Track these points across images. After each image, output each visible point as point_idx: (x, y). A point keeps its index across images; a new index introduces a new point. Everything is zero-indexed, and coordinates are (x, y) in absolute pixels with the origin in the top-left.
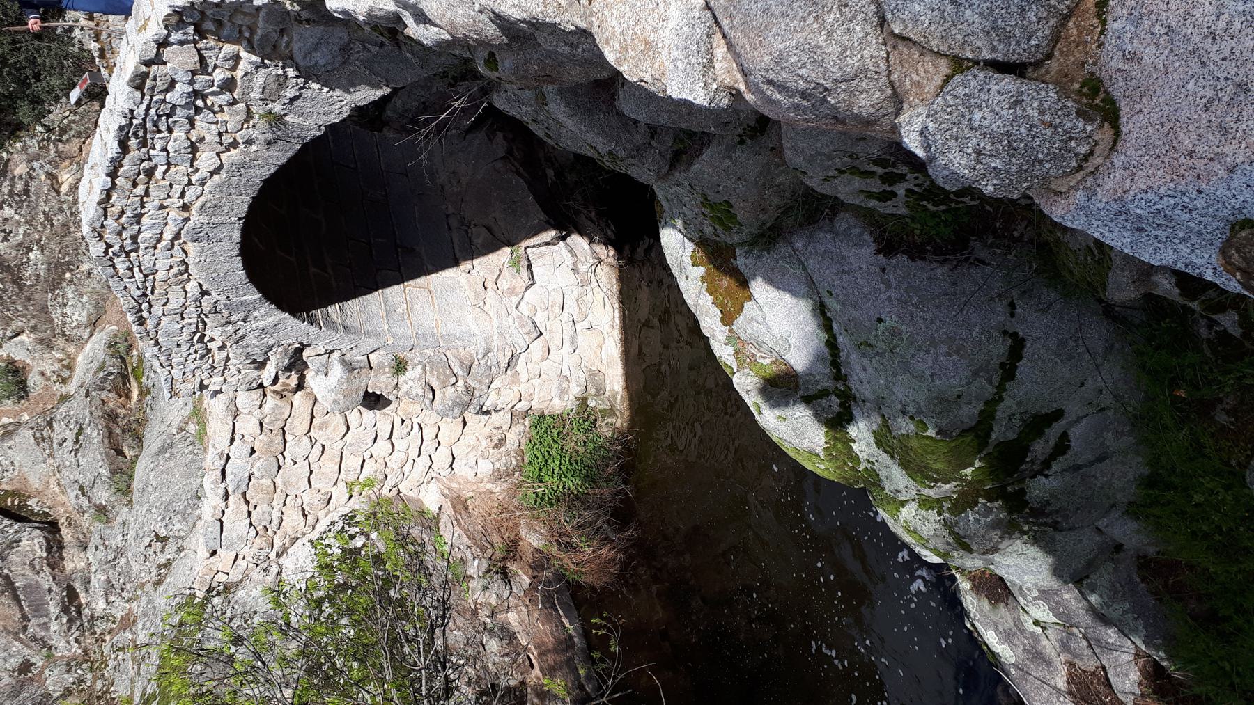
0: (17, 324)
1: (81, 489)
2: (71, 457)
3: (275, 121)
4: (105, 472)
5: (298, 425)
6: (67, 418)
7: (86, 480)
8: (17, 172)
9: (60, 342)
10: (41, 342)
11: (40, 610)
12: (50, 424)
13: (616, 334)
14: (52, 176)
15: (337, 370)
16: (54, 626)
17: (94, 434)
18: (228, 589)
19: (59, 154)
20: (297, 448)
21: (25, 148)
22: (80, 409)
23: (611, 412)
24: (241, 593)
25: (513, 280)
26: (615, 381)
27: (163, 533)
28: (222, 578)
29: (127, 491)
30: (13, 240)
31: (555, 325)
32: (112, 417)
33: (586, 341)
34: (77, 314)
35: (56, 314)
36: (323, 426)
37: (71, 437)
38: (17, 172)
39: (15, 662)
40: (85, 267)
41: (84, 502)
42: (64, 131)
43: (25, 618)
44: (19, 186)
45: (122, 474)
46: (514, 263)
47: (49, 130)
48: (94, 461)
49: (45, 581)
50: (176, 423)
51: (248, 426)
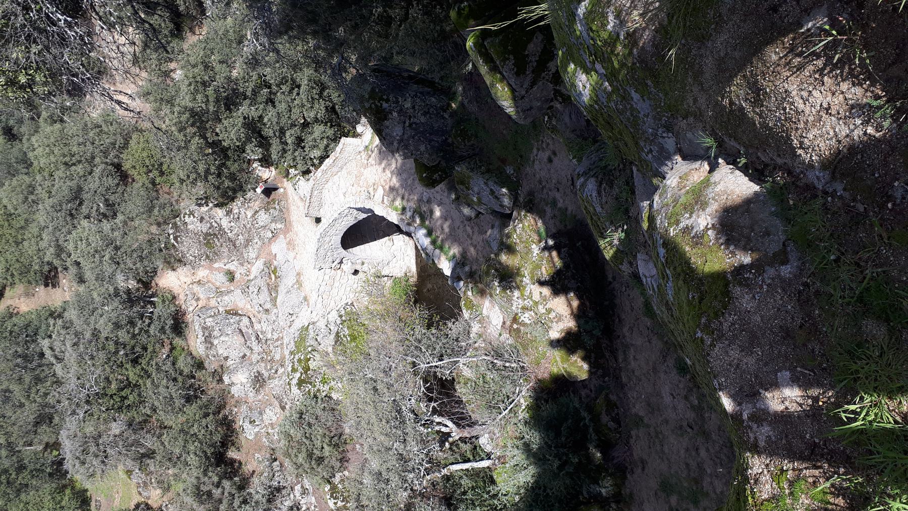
0: (233, 258)
1: (260, 305)
2: (256, 297)
3: (356, 218)
4: (268, 299)
5: (338, 278)
6: (255, 285)
7: (262, 303)
8: (235, 212)
9: (246, 264)
10: (240, 264)
11: (250, 339)
12: (248, 287)
13: (414, 257)
14: (245, 213)
15: (350, 264)
16: (254, 343)
17: (265, 289)
18: (313, 323)
19: (248, 207)
20: (337, 284)
21: (237, 205)
22: (261, 282)
23: (412, 277)
24: (317, 324)
25: (389, 243)
26: (414, 269)
27: (291, 313)
28: (312, 320)
29: (275, 305)
30: (233, 233)
31: (399, 254)
32: (268, 284)
33: (406, 258)
34: (252, 255)
35: (245, 255)
36: (343, 279)
37: (256, 290)
38: (235, 212)
39: (242, 354)
40: (255, 241)
41: (261, 309)
42: (250, 200)
43: (246, 341)
44: (236, 216)
45: (274, 301)
46: (389, 240)
47: (245, 199)
48: (264, 296)
49: (250, 331)
50: (291, 285)
51: (327, 277)
